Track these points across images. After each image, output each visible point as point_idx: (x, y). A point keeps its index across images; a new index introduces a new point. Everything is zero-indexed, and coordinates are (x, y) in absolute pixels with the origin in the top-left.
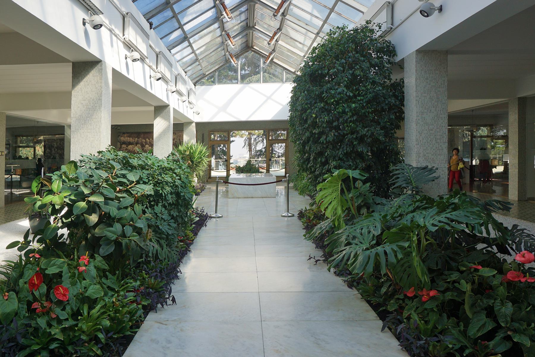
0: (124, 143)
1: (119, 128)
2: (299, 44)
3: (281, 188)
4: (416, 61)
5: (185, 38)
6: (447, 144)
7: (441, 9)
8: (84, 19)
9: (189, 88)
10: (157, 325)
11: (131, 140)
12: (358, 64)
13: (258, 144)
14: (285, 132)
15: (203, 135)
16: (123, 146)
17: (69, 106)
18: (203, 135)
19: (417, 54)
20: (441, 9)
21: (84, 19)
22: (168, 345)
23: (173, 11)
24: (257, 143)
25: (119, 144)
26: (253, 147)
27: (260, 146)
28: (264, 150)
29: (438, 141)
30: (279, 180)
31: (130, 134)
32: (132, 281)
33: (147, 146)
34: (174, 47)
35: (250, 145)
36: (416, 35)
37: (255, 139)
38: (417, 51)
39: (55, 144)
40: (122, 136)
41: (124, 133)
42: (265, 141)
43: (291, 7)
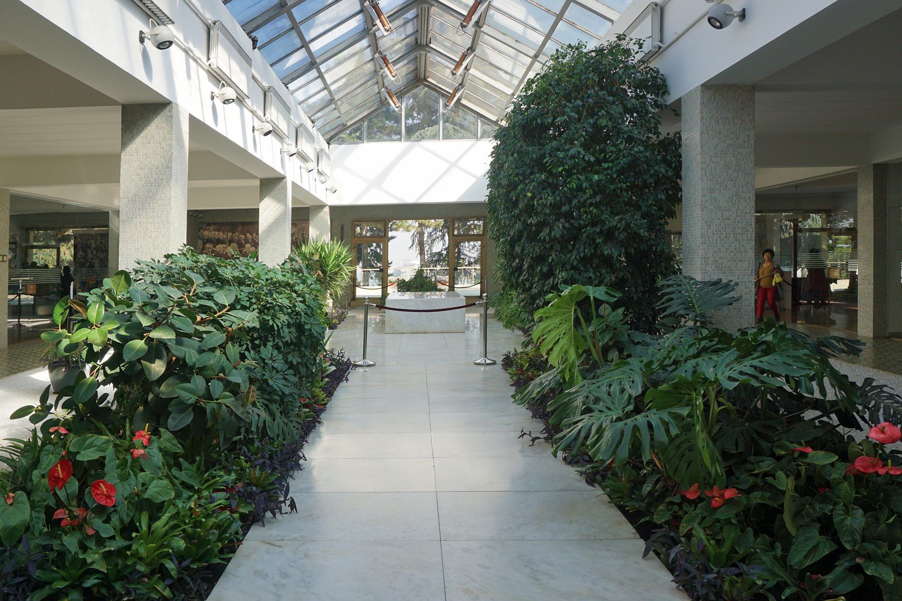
0: (209, 241)
1: (201, 215)
2: (505, 75)
3: (473, 317)
4: (702, 103)
5: (312, 64)
6: (753, 243)
7: (743, 16)
8: (141, 32)
9: (318, 148)
10: (265, 547)
11: (221, 235)
12: (603, 108)
13: (436, 243)
15: (342, 227)
16: (208, 245)
17: (116, 179)
18: (342, 227)
19: (702, 92)
20: (743, 16)
21: (141, 32)
22: (284, 581)
23: (292, 18)
24: (434, 240)
25: (200, 242)
26: (427, 248)
27: (439, 247)
28: (444, 252)
29: (739, 237)
30: (470, 303)
31: (220, 226)
32: (222, 473)
33: (248, 245)
34: (293, 80)
35: (421, 244)
36: (701, 59)
37: (430, 235)
38: (703, 85)
39: (93, 242)
40: (205, 230)
41: (209, 224)
42: (447, 238)
43: (491, 12)
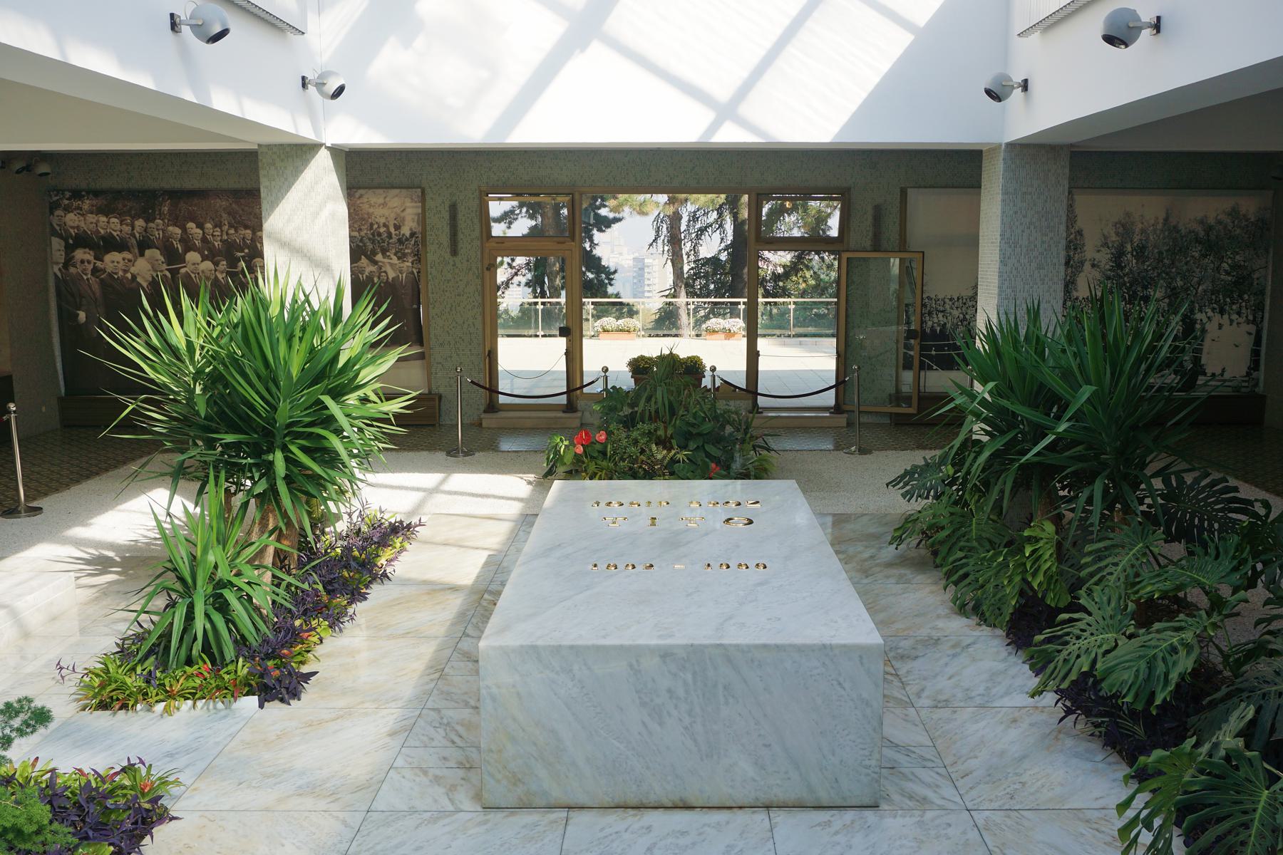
0: (82, 240)
1: (44, 168)
7: (1157, 26)
11: (113, 226)
13: (705, 237)
14: (498, 230)
15: (453, 209)
16: (80, 254)
18: (453, 209)
20: (1157, 26)
24: (702, 230)
25: (57, 244)
26: (687, 247)
27: (711, 246)
28: (724, 257)
31: (111, 201)
33: (192, 257)
35: (675, 241)
37: (694, 218)
40: (67, 209)
41: (77, 194)
42: (729, 227)
